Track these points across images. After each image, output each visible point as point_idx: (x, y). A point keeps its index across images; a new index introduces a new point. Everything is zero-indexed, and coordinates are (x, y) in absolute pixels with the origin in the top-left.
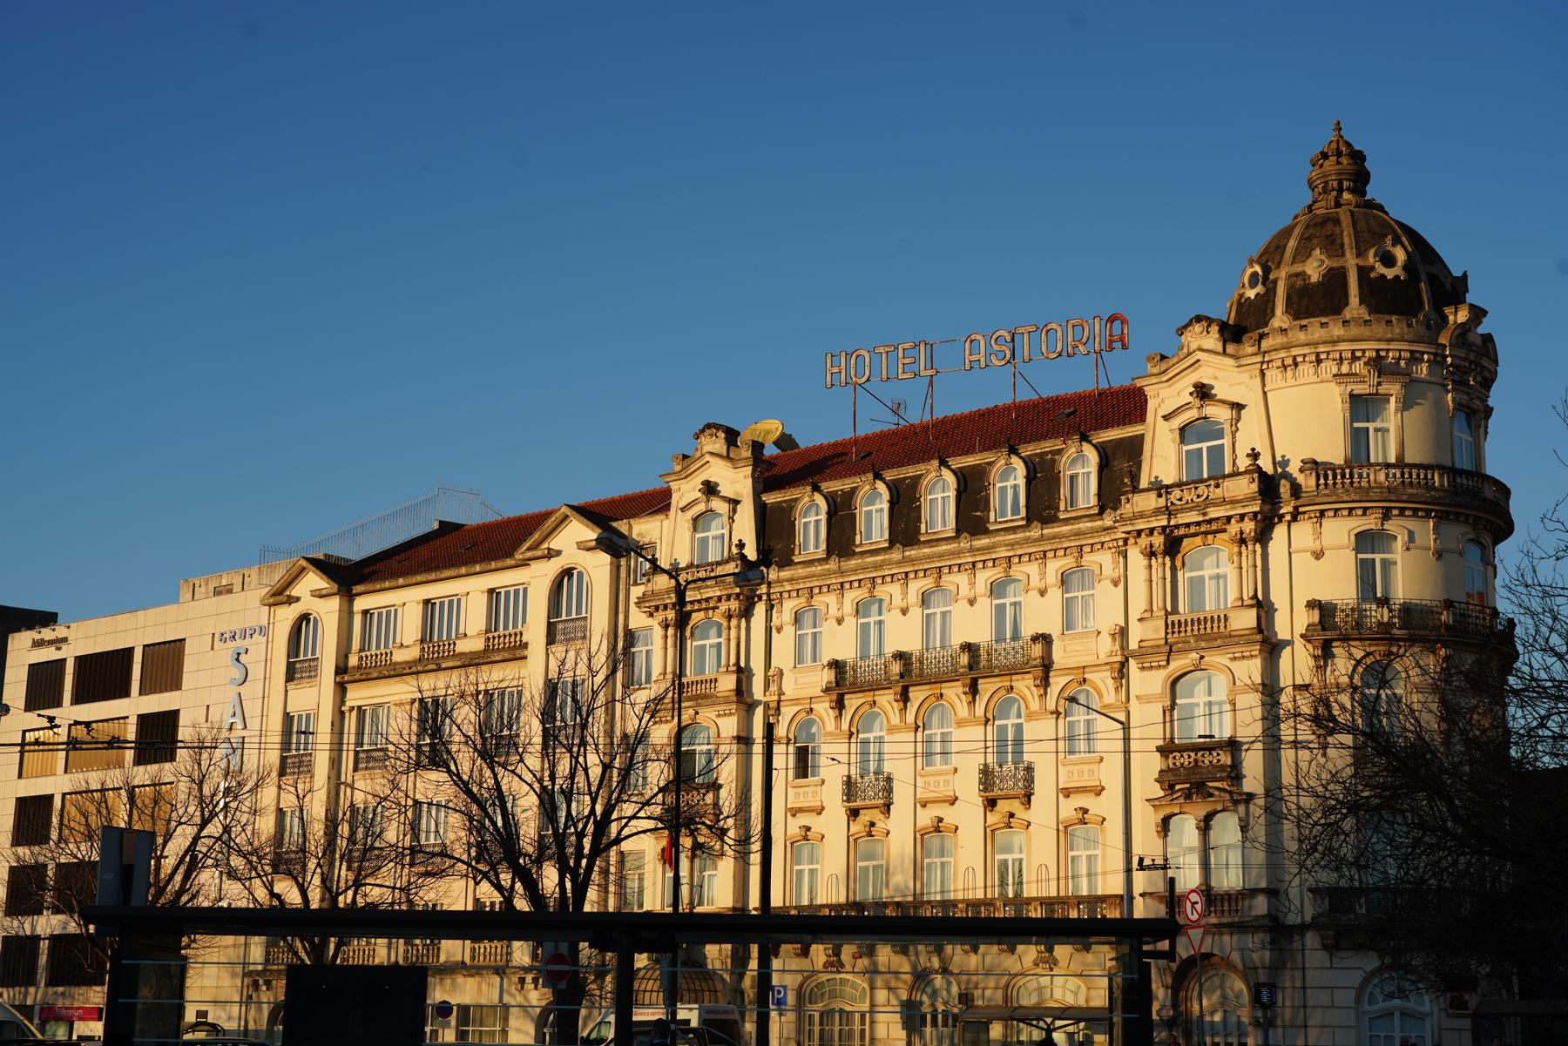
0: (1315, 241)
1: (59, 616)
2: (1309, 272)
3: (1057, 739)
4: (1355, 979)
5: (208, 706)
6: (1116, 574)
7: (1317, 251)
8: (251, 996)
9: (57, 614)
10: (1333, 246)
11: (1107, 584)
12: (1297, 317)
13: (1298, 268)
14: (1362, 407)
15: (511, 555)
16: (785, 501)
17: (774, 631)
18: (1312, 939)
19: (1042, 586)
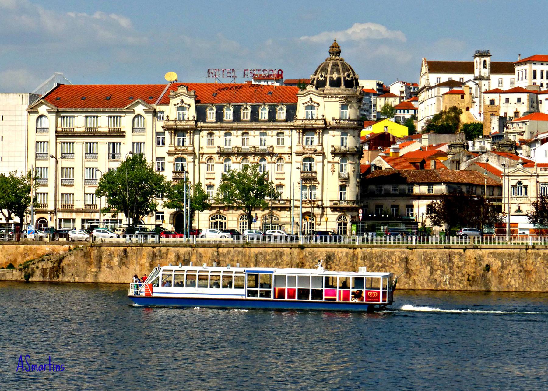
0: (334, 70)
1: (522, 99)
2: (334, 77)
3: (509, 203)
4: (336, 216)
5: (2, 137)
6: (289, 134)
7: (335, 73)
8: (296, 383)
9: (518, 98)
10: (338, 71)
11: (287, 137)
12: (331, 87)
13: (331, 76)
14: (343, 107)
15: (124, 106)
16: (202, 106)
17: (201, 137)
18: (329, 209)
19: (254, 135)
